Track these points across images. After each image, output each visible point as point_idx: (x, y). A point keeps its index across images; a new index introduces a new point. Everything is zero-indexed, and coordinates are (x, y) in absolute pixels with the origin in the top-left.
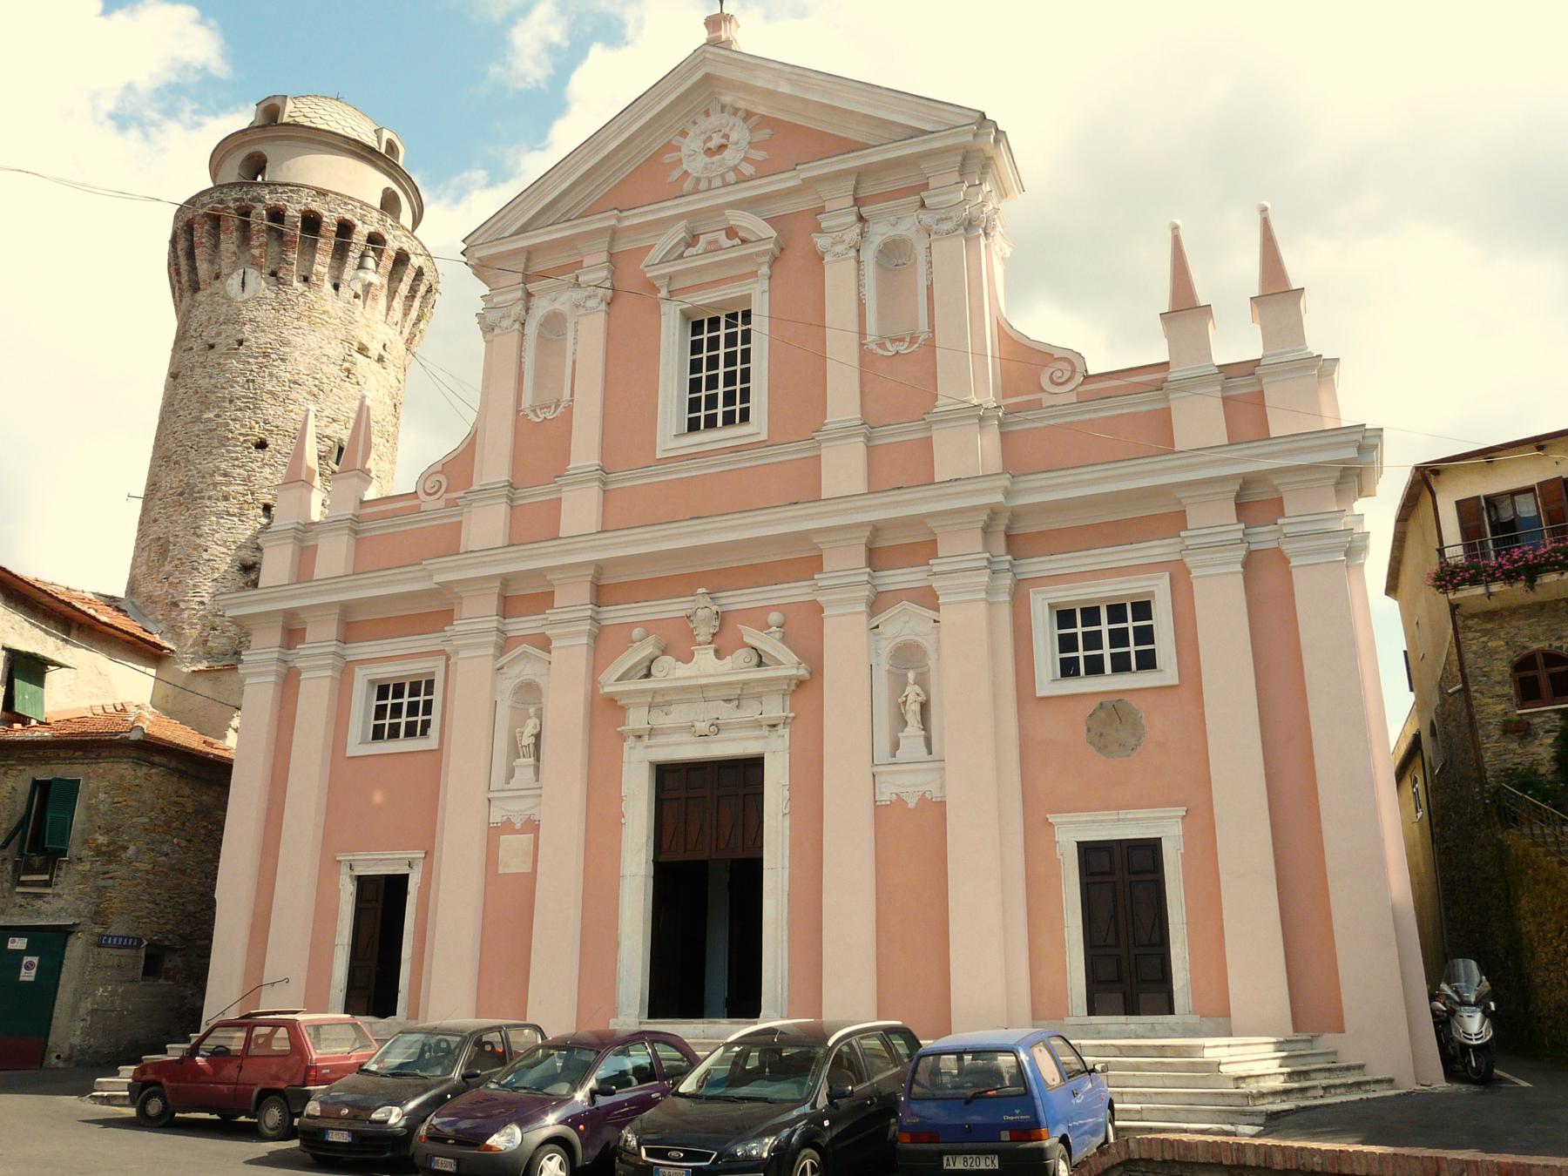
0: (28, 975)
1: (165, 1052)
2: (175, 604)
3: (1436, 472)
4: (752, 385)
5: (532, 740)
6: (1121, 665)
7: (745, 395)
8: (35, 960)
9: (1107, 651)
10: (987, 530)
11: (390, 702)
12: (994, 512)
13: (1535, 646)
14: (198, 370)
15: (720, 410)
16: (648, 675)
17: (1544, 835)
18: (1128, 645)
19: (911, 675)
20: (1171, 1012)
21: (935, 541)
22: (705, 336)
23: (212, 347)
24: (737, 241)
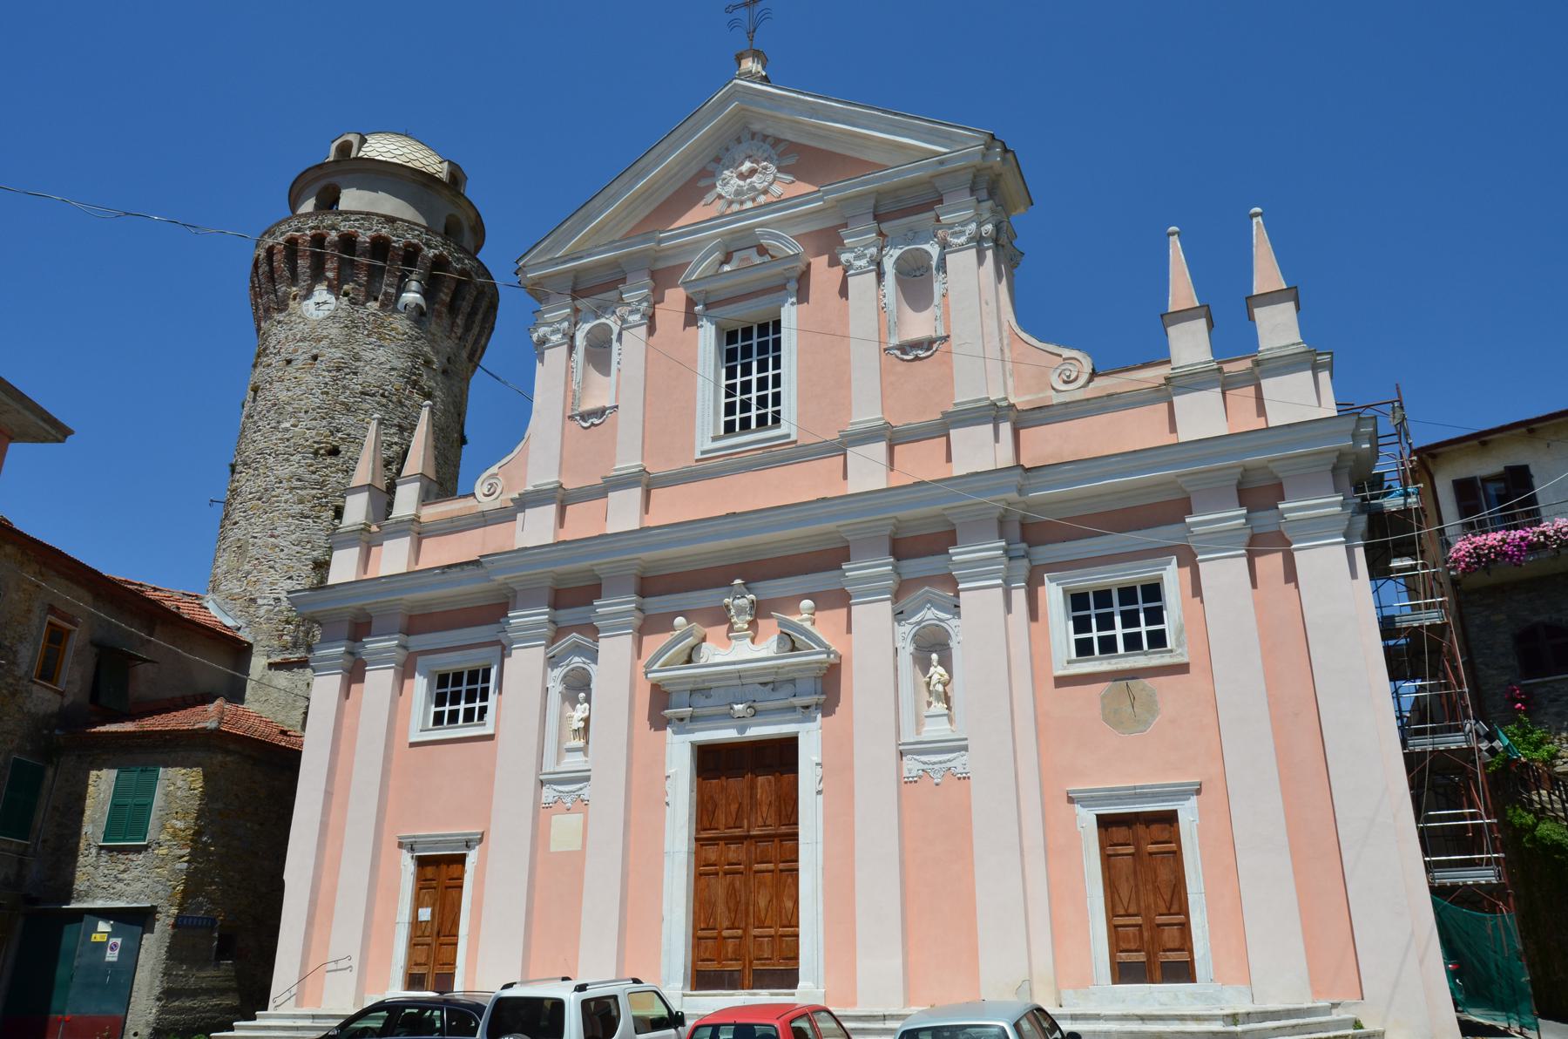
0: (112, 956)
1: (232, 1029)
2: (253, 600)
3: (1434, 457)
4: (783, 389)
5: (582, 724)
6: (1133, 643)
7: (777, 399)
8: (119, 941)
9: (1119, 631)
10: (1335, 470)
11: (449, 690)
12: (1342, 455)
13: (1536, 619)
14: (276, 385)
15: (754, 413)
16: (689, 660)
17: (1551, 801)
18: (1090, 631)
19: (934, 656)
20: (1193, 980)
21: (954, 531)
22: (739, 345)
23: (289, 362)
24: (767, 258)
